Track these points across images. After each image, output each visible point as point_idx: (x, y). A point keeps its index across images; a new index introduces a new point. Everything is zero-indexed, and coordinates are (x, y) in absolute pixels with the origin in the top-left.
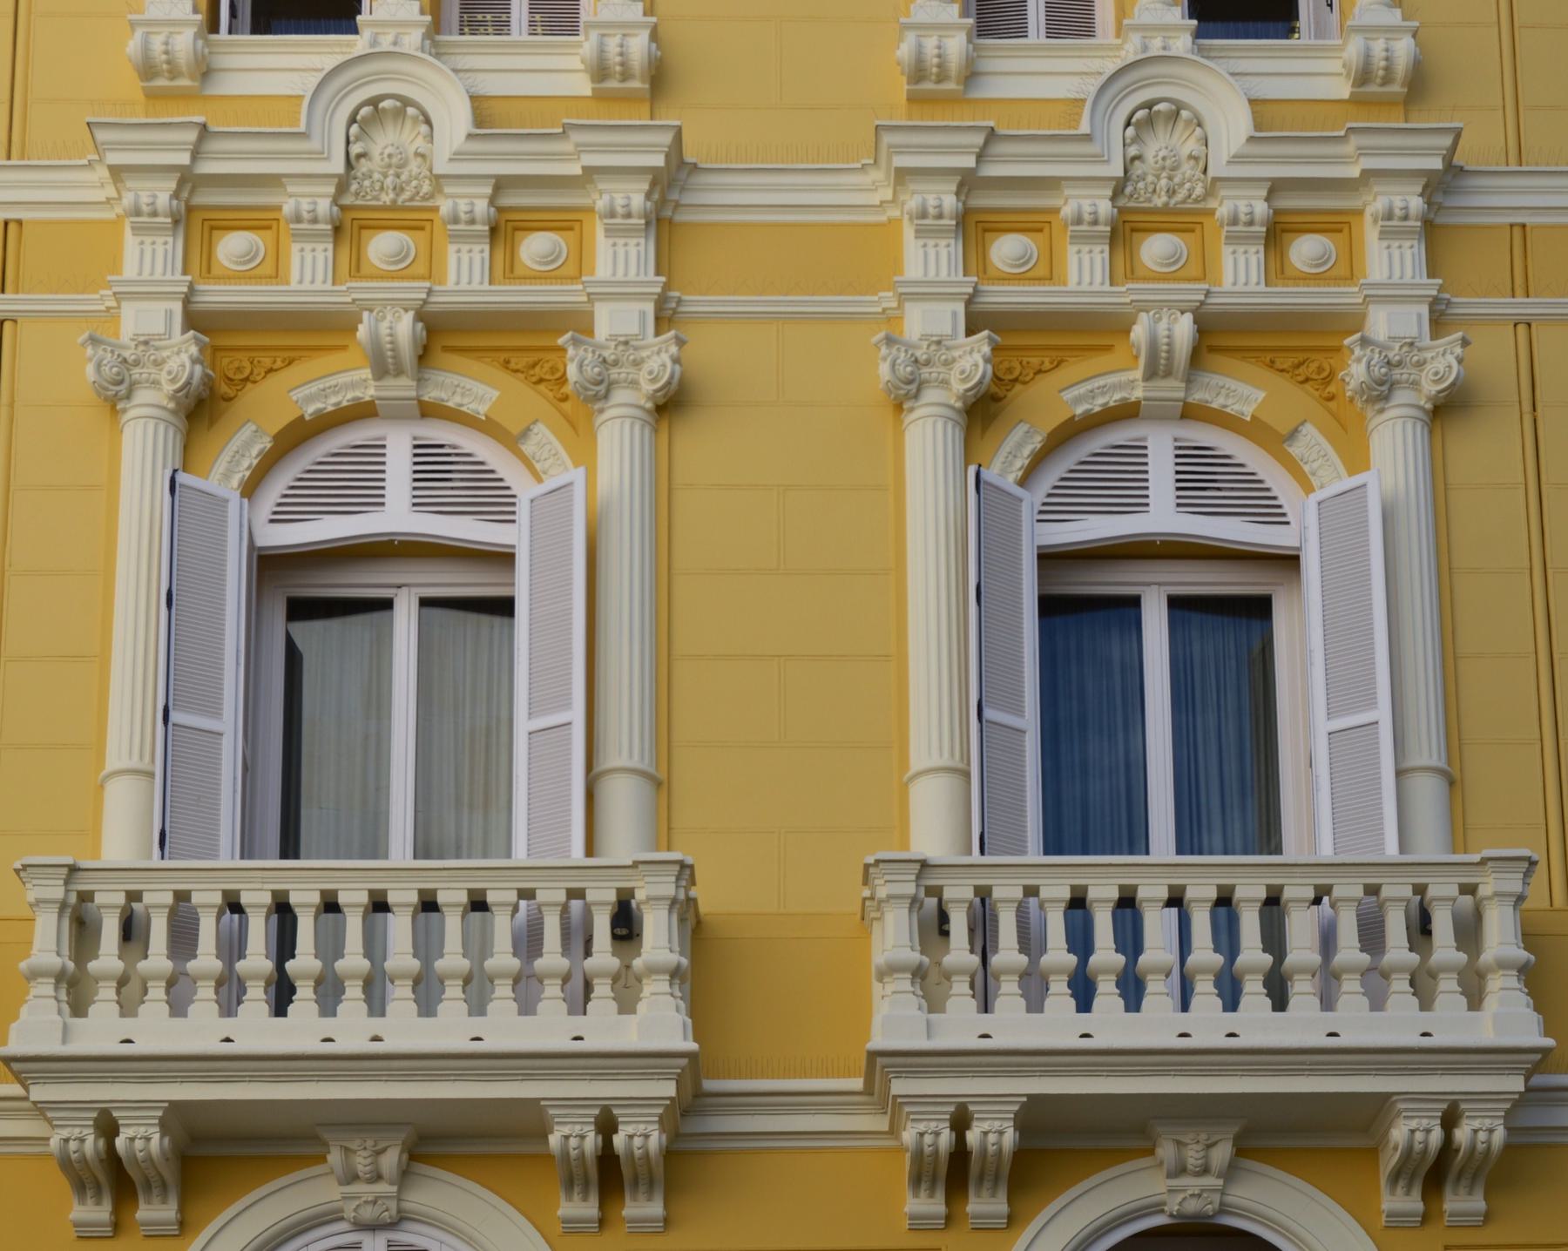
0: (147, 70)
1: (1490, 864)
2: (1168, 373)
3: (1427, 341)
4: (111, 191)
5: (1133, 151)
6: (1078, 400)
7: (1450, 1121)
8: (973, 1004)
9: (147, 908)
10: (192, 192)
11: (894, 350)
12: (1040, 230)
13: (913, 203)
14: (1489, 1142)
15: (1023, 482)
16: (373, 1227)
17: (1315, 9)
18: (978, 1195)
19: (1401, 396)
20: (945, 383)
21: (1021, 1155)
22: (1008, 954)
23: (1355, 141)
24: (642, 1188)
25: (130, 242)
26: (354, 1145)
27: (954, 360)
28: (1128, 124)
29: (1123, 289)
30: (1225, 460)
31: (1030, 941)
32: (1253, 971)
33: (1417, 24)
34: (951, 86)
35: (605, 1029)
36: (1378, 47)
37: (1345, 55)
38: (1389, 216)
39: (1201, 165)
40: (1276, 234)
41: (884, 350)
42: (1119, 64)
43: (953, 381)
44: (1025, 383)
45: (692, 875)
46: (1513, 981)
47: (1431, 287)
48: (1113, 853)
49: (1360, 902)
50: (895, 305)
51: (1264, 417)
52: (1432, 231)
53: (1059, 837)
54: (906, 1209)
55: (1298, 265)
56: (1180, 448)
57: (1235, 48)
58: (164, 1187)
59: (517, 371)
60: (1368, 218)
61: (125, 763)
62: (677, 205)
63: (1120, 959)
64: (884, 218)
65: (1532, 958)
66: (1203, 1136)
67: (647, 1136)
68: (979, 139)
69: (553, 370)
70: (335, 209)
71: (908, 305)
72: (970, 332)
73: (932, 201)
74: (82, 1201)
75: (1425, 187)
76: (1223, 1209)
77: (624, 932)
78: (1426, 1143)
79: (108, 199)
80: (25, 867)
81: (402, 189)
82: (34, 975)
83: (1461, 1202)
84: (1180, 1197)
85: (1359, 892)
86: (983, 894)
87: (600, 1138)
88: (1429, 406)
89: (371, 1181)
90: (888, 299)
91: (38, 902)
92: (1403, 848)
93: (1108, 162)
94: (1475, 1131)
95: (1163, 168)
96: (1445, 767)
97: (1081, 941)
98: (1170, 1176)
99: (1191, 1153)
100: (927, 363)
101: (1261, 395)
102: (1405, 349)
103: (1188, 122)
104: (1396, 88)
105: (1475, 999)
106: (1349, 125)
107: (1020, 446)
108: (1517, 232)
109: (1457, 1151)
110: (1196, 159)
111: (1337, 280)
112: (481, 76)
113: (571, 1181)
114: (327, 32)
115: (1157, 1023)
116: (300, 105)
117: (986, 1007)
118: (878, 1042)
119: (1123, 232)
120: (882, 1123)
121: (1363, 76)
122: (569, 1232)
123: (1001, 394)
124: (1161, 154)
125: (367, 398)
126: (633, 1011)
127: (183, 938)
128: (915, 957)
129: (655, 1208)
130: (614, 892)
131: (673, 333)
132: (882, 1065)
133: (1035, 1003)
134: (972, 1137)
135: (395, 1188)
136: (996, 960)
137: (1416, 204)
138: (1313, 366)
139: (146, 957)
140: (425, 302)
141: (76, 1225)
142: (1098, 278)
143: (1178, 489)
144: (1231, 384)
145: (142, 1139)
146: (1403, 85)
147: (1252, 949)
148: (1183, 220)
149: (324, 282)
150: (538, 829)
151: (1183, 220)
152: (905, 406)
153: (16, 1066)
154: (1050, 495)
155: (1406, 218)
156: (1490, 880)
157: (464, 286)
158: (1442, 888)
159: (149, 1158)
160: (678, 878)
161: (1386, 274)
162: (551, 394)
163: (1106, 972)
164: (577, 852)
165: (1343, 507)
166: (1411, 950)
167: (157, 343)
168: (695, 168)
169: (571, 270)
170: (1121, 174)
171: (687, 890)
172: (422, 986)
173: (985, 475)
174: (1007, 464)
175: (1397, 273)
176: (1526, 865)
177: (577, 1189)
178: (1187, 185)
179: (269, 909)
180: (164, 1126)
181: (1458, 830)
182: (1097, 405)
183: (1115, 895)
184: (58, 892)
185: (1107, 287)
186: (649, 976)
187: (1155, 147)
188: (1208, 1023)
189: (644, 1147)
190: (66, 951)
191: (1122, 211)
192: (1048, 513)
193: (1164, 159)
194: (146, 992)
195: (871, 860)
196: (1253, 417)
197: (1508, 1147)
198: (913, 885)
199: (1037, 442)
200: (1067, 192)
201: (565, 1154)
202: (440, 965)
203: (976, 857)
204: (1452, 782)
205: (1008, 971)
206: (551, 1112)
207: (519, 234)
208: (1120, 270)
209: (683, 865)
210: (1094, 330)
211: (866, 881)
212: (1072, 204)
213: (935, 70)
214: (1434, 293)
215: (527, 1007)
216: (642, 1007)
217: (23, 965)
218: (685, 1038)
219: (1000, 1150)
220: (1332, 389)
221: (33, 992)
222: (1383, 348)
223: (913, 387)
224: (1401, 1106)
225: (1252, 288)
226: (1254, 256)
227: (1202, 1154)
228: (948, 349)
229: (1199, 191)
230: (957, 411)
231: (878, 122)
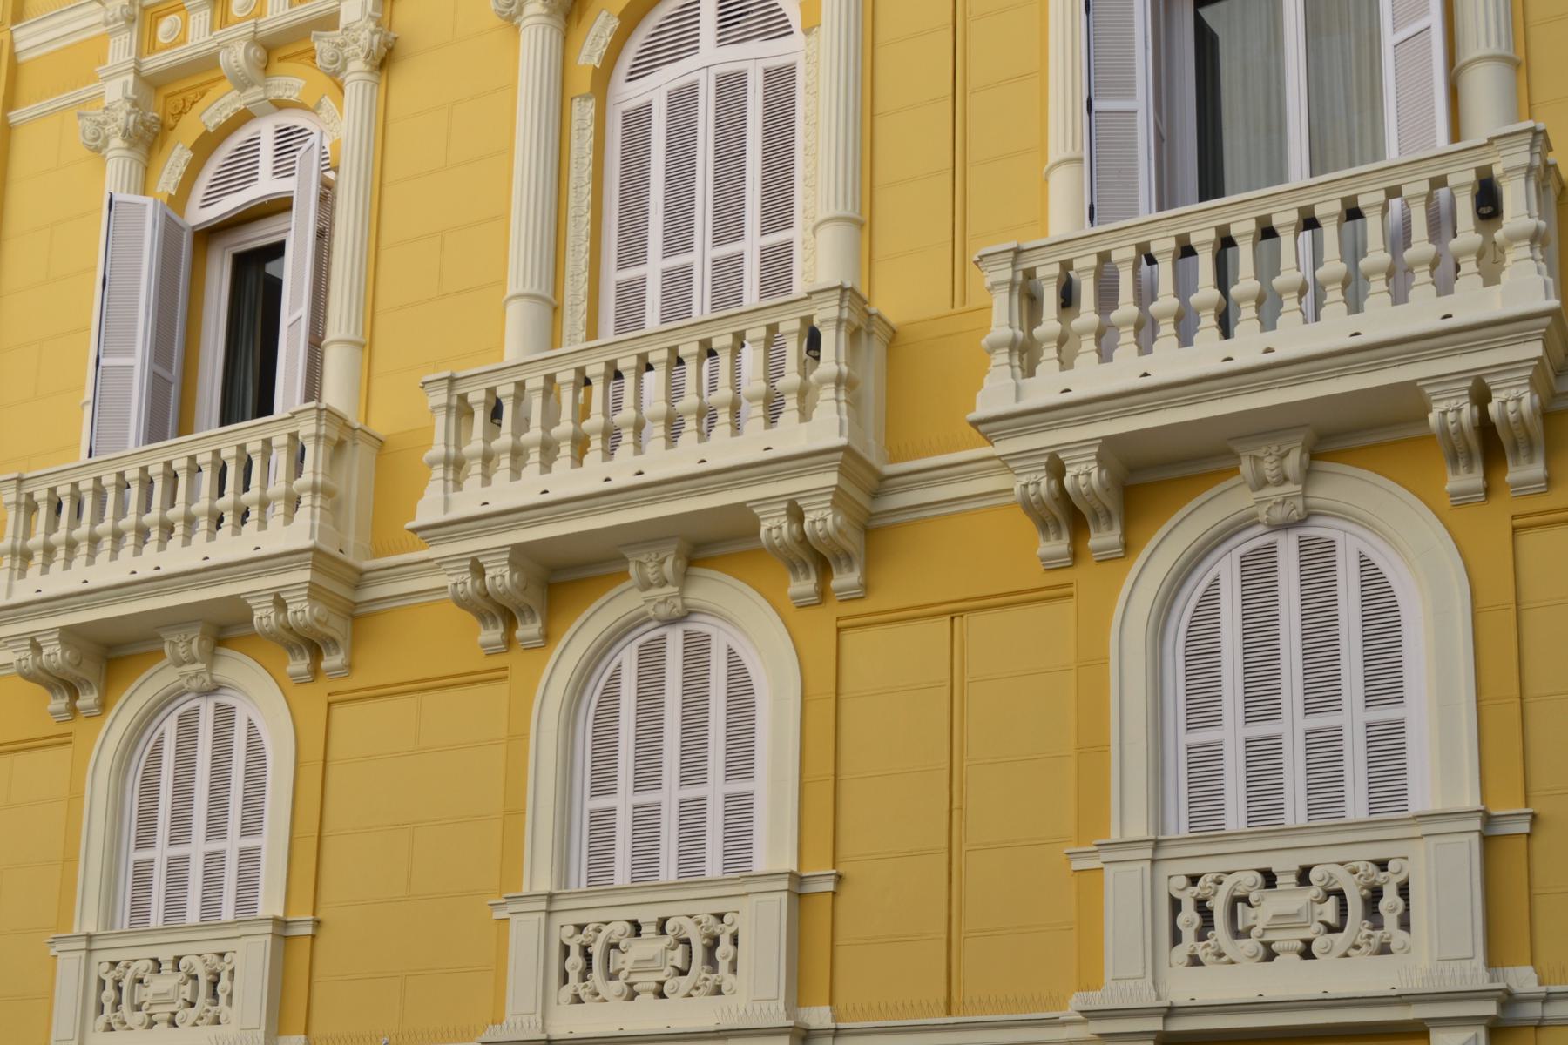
8: (1216, 332)
16: (1284, 526)
18: (1098, 530)
21: (1547, 414)
24: (1523, 452)
35: (1474, 302)
45: (1547, 140)
58: (1109, 515)
61: (1062, 155)
67: (1519, 400)
74: (1047, 539)
77: (1486, 210)
80: (981, 257)
82: (993, 348)
84: (1265, 507)
86: (1104, 257)
87: (1476, 409)
91: (994, 285)
99: (1267, 465)
113: (794, 566)
122: (1457, 505)
126: (1497, 281)
127: (1107, 296)
129: (1537, 470)
130: (1338, 203)
132: (990, 428)
135: (1299, 487)
136: (1234, 291)
139: (1455, 236)
141: (483, 646)
144: (283, 80)
145: (1084, 474)
150: (1410, 124)
153: (982, 428)
159: (1091, 491)
160: (1532, 146)
164: (1442, 142)
171: (1543, 156)
172: (1350, 289)
177: (1461, 463)
179: (1297, 225)
180: (1101, 460)
184: (1007, 274)
186: (1509, 245)
189: (1457, 420)
190: (1016, 323)
194: (1458, 268)
198: (1527, 155)
201: (1444, 429)
202: (1194, 299)
203: (1088, 230)
206: (1428, 391)
208: (218, 22)
209: (1535, 132)
215: (1399, 297)
216: (1505, 276)
218: (1547, 297)
221: (994, 362)
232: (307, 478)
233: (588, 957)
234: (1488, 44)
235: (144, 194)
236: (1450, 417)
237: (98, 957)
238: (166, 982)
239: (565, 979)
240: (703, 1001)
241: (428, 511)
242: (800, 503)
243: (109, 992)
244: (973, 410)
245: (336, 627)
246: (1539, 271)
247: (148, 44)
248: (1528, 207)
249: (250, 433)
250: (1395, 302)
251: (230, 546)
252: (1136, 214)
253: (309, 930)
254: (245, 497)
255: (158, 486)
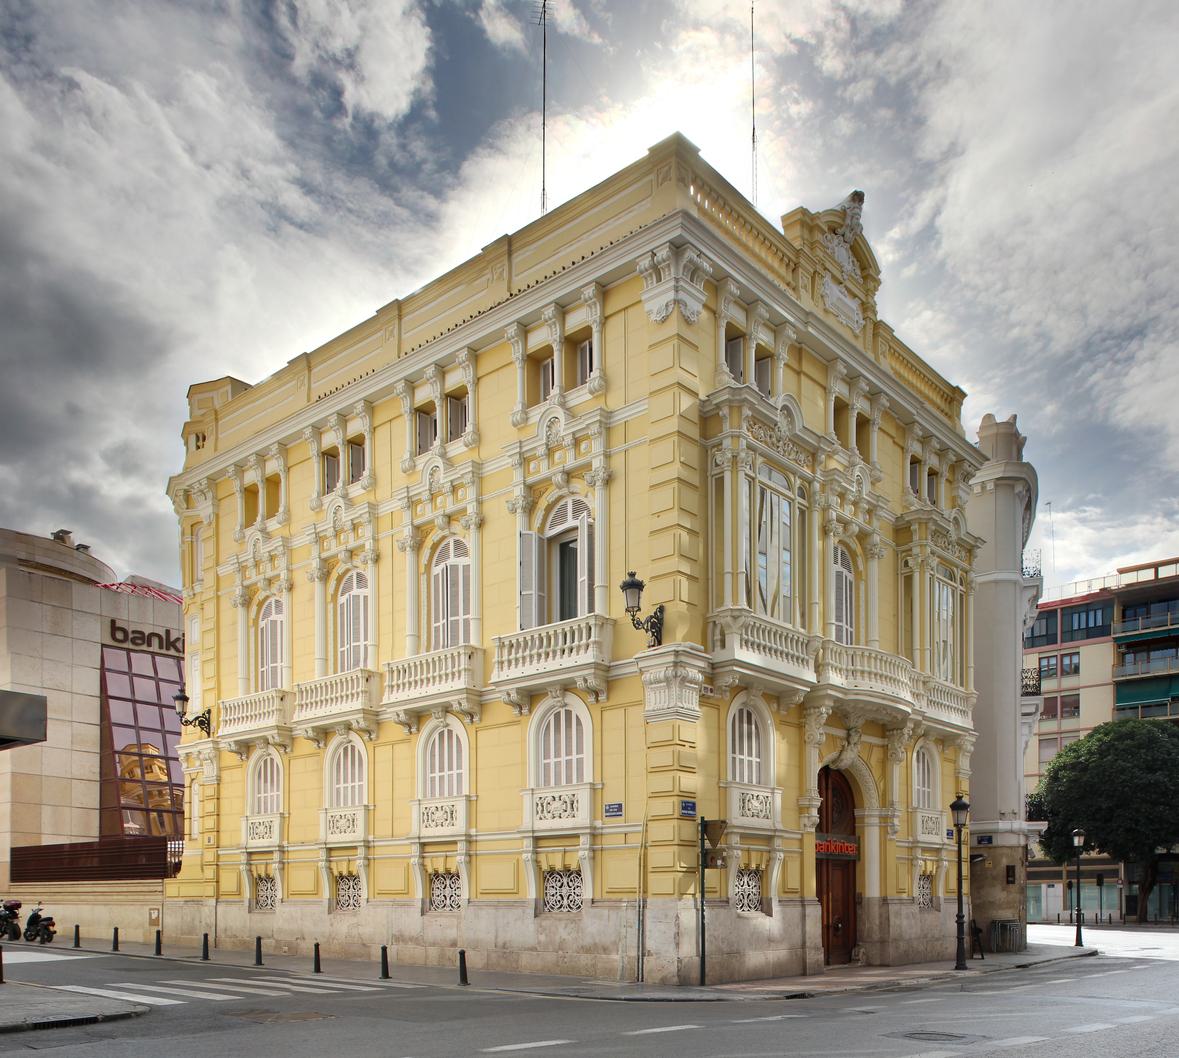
232: (592, 639)
233: (543, 806)
235: (530, 529)
237: (535, 796)
238: (557, 804)
239: (538, 812)
240: (571, 819)
241: (494, 679)
243: (426, 816)
245: (373, 727)
247: (322, 549)
249: (567, 624)
251: (568, 661)
253: (600, 787)
254: (540, 651)
255: (553, 639)
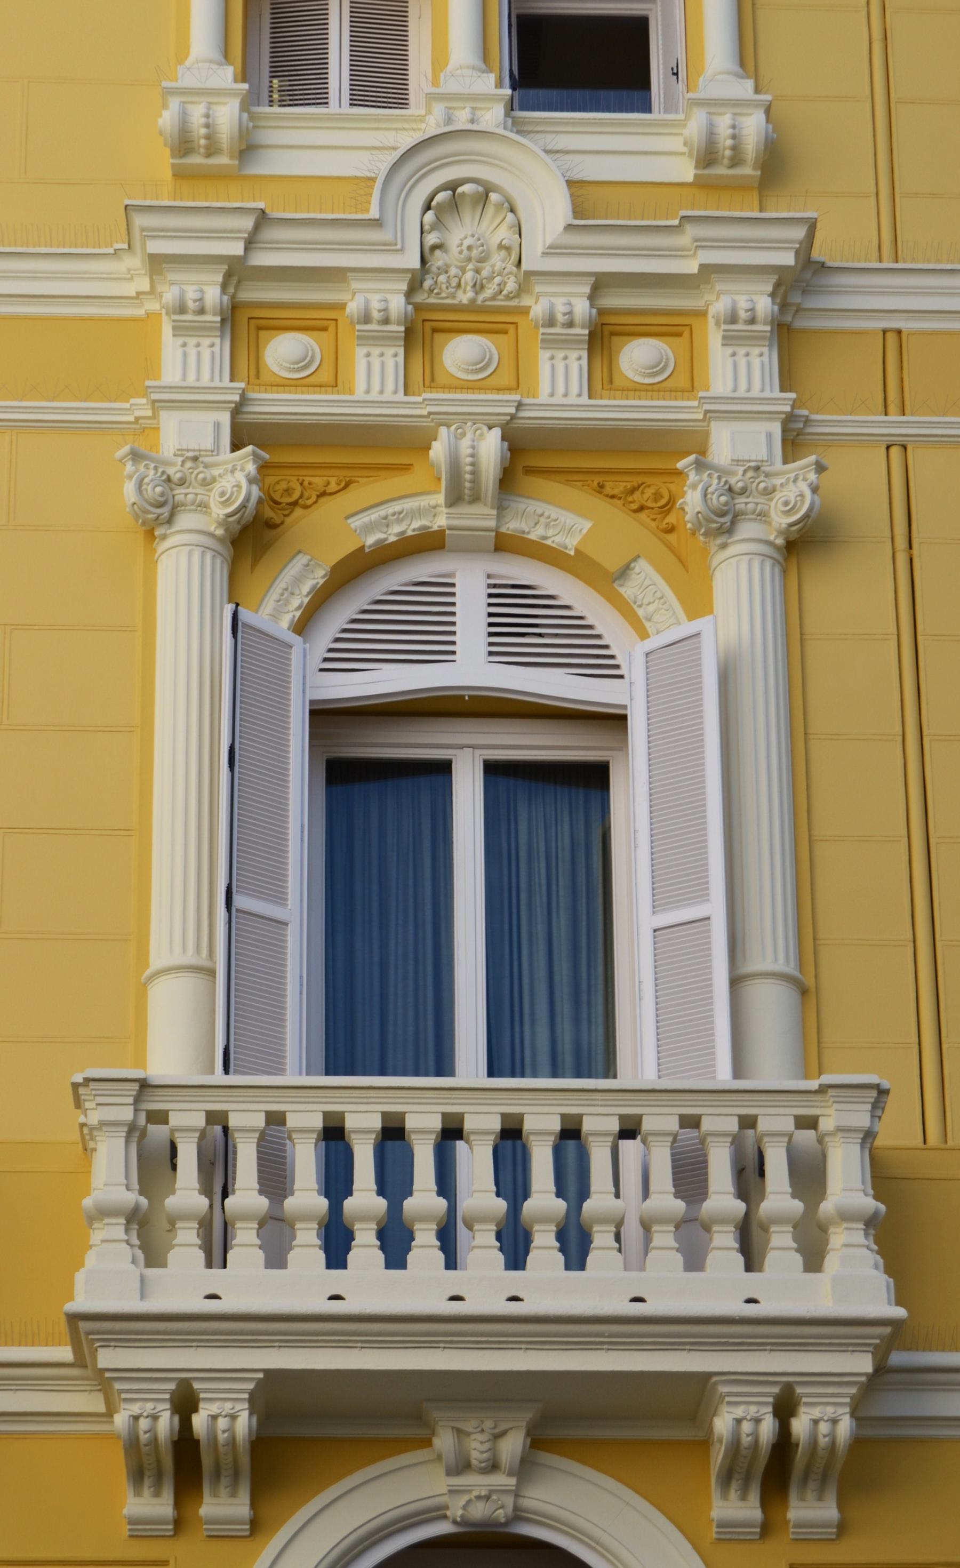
0: (183, 144)
1: (831, 1092)
2: (476, 498)
3: (778, 465)
4: (143, 284)
5: (432, 239)
6: (370, 528)
7: (785, 1408)
9: (173, 1131)
10: (237, 287)
11: (142, 468)
12: (325, 329)
13: (170, 295)
14: (832, 1435)
15: (302, 627)
17: (665, 78)
18: (215, 1494)
19: (747, 529)
20: (203, 507)
21: (260, 1444)
22: (247, 1195)
23: (691, 231)
24: (224, 1481)
25: (170, 346)
26: (468, 1426)
27: (214, 480)
28: (428, 207)
29: (420, 399)
30: (548, 601)
31: (275, 1179)
32: (543, 1220)
33: (769, 97)
34: (223, 160)
36: (723, 124)
37: (686, 132)
38: (733, 318)
39: (514, 257)
40: (602, 337)
41: (129, 467)
42: (417, 137)
43: (212, 505)
44: (306, 507)
46: (858, 1235)
47: (784, 402)
48: (417, 1074)
49: (675, 1136)
50: (149, 413)
51: (589, 551)
52: (786, 335)
53: (344, 1049)
54: (125, 1511)
55: (630, 374)
56: (495, 586)
57: (567, 123)
59: (613, 497)
60: (711, 321)
62: (799, 310)
63: (561, 1205)
64: (140, 312)
65: (882, 1207)
66: (488, 1424)
68: (248, 223)
69: (657, 496)
70: (410, 307)
71: (163, 414)
72: (236, 446)
73: (191, 294)
74: (138, 1493)
75: (777, 285)
76: (519, 1515)
78: (755, 1435)
79: (138, 294)
80: (87, 1081)
81: (482, 287)
82: (103, 1213)
83: (810, 1509)
85: (673, 1124)
87: (176, 1419)
88: (780, 541)
89: (485, 1471)
90: (140, 407)
92: (738, 1071)
93: (402, 250)
94: (739, 1421)
95: (469, 259)
96: (797, 974)
97: (337, 1181)
98: (450, 1472)
99: (474, 1445)
100: (182, 482)
101: (587, 525)
102: (750, 474)
103: (499, 207)
104: (748, 170)
105: (813, 1259)
106: (683, 213)
107: (298, 580)
108: (891, 338)
109: (797, 1445)
110: (508, 249)
111: (675, 392)
112: (577, 158)
113: (735, 1471)
114: (632, 110)
115: (424, 1285)
116: (372, 188)
117: (451, 1263)
118: (81, 1303)
119: (420, 332)
120: (95, 1403)
121: (708, 156)
123: (278, 521)
124: (467, 243)
125: (435, 528)
128: (131, 1198)
130: (438, 1119)
131: (813, 458)
132: (89, 1329)
133: (276, 1258)
134: (800, 1426)
137: (764, 305)
138: (649, 492)
140: (513, 417)
141: (132, 1521)
142: (574, 389)
143: (491, 634)
144: (534, 506)
145: (226, 1417)
146: (754, 168)
147: (545, 1195)
148: (493, 319)
149: (395, 392)
151: (493, 319)
152: (157, 533)
154: (337, 640)
155: (752, 321)
156: (831, 1111)
157: (375, 396)
158: (775, 1121)
161: (730, 386)
162: (653, 524)
163: (365, 1218)
165: (679, 658)
166: (498, 1195)
167: (207, 460)
168: (822, 267)
169: (682, 380)
170: (416, 264)
173: (246, 615)
174: (283, 602)
175: (743, 386)
176: (874, 1093)
178: (497, 280)
181: (811, 1047)
182: (392, 534)
183: (557, 1126)
185: (585, 400)
187: (460, 234)
188: (484, 1282)
189: (152, 1430)
191: (418, 308)
192: (335, 661)
193: (470, 248)
195: (79, 1078)
196: (577, 550)
197: (858, 1442)
199: (318, 577)
200: (354, 285)
202: (290, 1203)
203: (219, 1077)
204: (804, 990)
205: (780, 1220)
207: (439, 337)
210: (385, 446)
211: (78, 1104)
212: (359, 298)
213: (203, 142)
214: (788, 409)
217: (88, 1202)
219: (234, 1439)
220: (671, 519)
222: (723, 472)
223: (165, 511)
224: (723, 1389)
225: (572, 399)
226: (575, 362)
227: (487, 1446)
228: (206, 466)
229: (511, 286)
230: (220, 540)
231: (127, 202)
234: (776, 959)
236: (824, 1428)
242: (196, 1386)
244: (71, 1298)
246: (134, 1261)
248: (127, 1176)
250: (389, 1265)
252: (280, 1071)
